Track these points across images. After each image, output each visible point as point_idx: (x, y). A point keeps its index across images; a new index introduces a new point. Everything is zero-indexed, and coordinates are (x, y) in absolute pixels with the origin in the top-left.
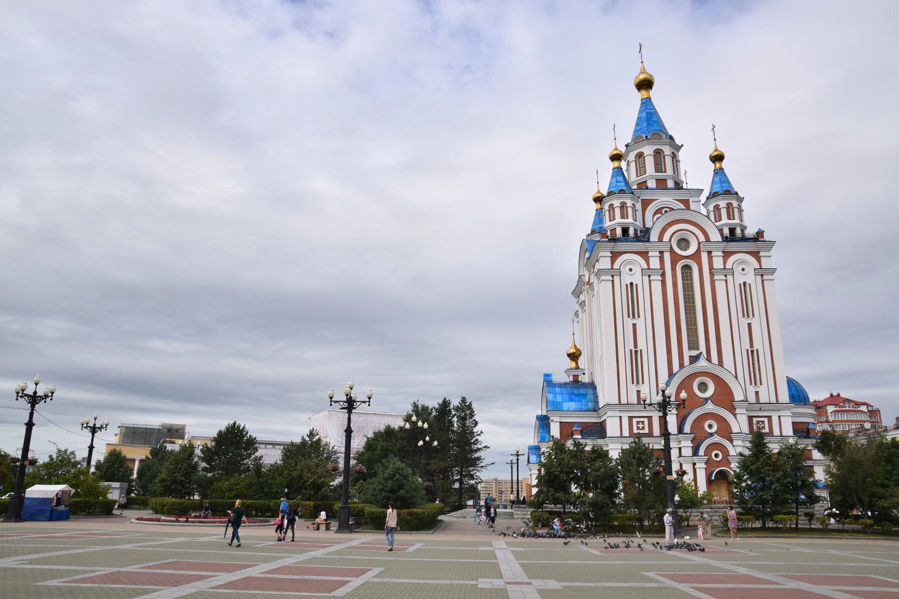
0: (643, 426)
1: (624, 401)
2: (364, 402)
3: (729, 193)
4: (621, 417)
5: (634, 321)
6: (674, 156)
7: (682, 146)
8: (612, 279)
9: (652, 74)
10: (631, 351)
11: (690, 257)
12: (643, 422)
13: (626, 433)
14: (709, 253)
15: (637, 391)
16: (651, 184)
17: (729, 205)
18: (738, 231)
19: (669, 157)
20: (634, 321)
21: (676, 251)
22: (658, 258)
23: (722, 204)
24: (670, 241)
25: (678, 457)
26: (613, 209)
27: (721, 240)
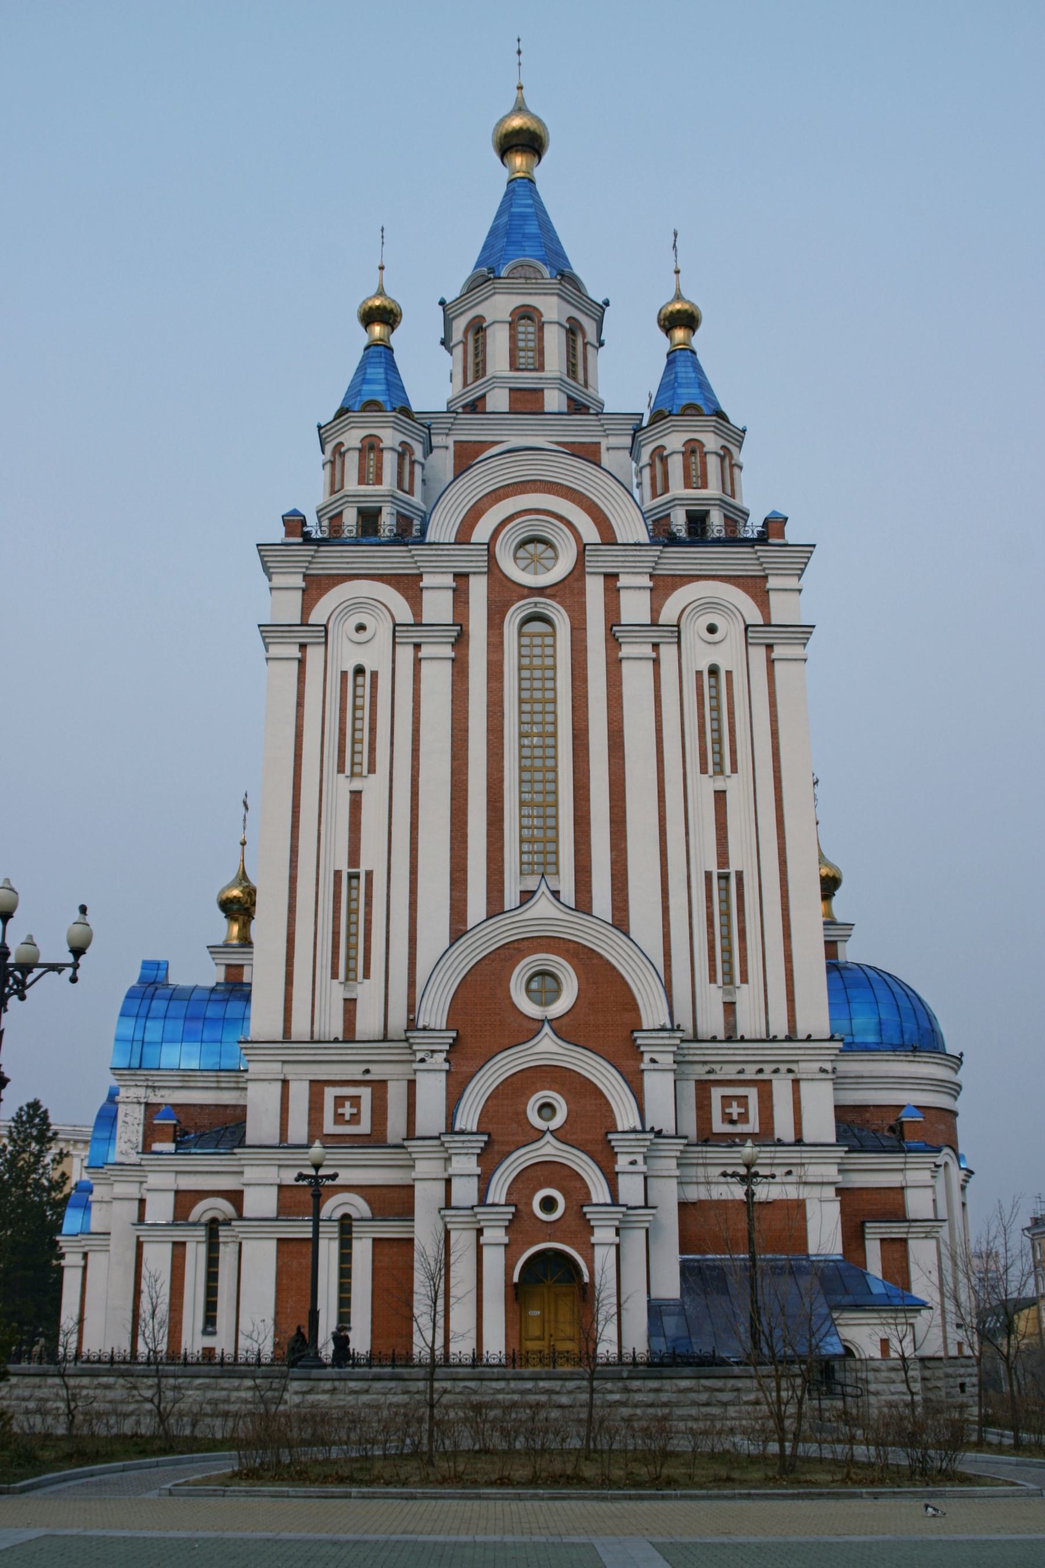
0: (355, 1111)
1: (300, 1028)
2: (56, 968)
3: (694, 412)
4: (285, 1082)
5: (357, 785)
6: (725, 455)
7: (607, 303)
8: (299, 655)
9: (545, 120)
11: (548, 591)
12: (356, 1100)
13: (299, 1131)
14: (611, 577)
15: (345, 1000)
16: (498, 400)
17: (693, 449)
18: (716, 518)
19: (556, 327)
20: (357, 785)
21: (514, 578)
23: (674, 441)
24: (490, 546)
25: (134, 1224)
26: (664, 460)
27: (648, 541)
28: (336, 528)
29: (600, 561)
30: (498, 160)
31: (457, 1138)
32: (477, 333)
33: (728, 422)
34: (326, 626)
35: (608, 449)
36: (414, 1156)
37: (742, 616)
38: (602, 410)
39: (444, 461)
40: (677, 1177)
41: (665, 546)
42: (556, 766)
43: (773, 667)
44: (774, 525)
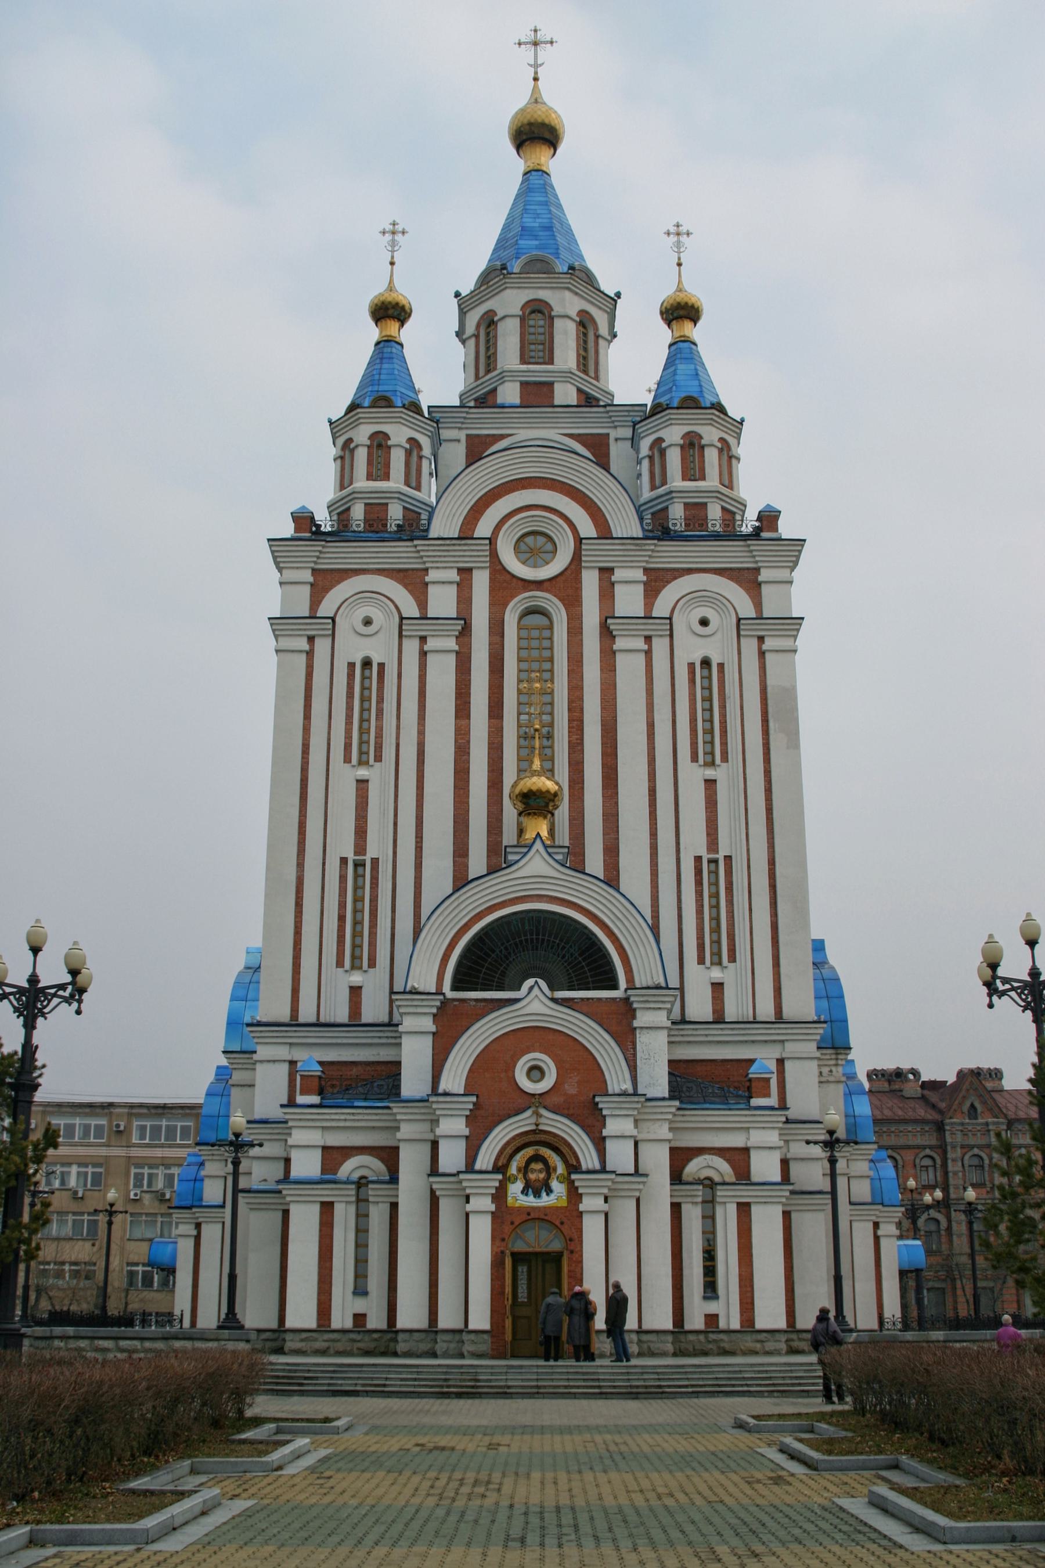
1: (307, 1014)
3: (415, 410)
8: (646, 647)
10: (698, 859)
14: (606, 572)
16: (510, 393)
17: (692, 445)
18: (714, 512)
22: (308, 588)
23: (673, 434)
24: (492, 541)
26: (663, 453)
28: (345, 523)
29: (595, 555)
30: (514, 152)
31: (441, 1099)
32: (489, 326)
33: (726, 414)
34: (333, 619)
35: (616, 440)
36: (399, 1117)
37: (735, 609)
38: (612, 400)
39: (455, 454)
40: (669, 1141)
41: (659, 539)
42: (553, 756)
43: (764, 658)
44: (769, 518)
